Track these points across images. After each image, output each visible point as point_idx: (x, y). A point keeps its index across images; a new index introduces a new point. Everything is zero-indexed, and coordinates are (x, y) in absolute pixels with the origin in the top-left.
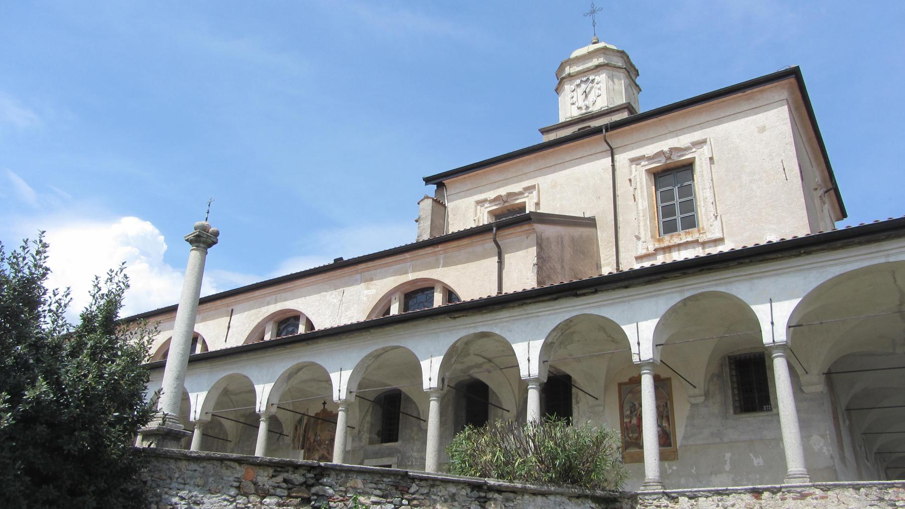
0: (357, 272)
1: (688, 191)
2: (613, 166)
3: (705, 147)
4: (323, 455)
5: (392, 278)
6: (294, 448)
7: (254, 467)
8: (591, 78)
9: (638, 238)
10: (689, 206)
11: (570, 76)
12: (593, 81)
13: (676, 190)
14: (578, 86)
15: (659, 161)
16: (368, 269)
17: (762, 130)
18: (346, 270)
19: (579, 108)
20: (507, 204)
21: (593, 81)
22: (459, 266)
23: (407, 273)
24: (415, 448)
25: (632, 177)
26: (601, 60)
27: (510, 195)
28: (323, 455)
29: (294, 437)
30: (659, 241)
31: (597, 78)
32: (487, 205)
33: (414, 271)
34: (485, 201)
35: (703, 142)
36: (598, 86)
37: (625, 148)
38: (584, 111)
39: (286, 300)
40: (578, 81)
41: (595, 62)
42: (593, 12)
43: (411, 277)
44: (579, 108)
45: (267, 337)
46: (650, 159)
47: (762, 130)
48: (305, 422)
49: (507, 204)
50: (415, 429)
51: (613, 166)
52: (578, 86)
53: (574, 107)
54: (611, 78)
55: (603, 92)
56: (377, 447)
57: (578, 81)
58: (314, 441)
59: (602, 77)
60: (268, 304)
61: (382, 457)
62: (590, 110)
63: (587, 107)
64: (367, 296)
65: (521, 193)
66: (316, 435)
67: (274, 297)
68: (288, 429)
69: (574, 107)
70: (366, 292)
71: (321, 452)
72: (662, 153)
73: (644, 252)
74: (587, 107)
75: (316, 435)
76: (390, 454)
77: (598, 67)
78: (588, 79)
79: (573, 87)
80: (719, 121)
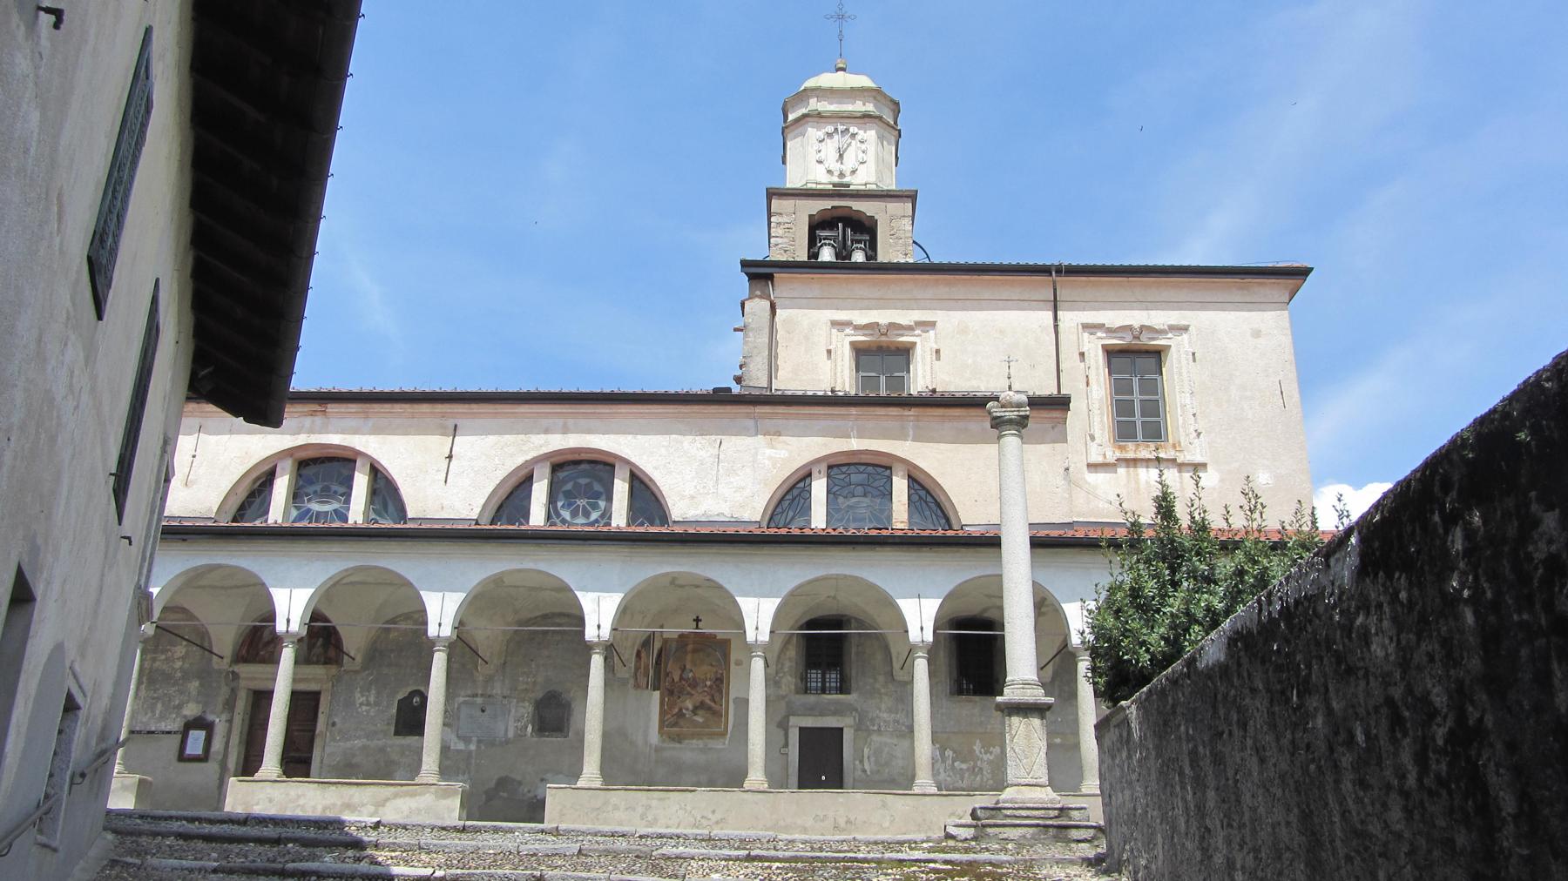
0: (748, 416)
1: (1153, 388)
2: (1056, 326)
3: (1185, 336)
4: (702, 703)
5: (820, 440)
6: (637, 686)
7: (1026, 716)
8: (853, 129)
9: (1093, 438)
10: (1154, 408)
11: (819, 116)
12: (853, 136)
13: (1136, 380)
14: (830, 135)
15: (1122, 338)
16: (771, 417)
17: (1257, 334)
18: (729, 408)
19: (829, 172)
20: (883, 338)
21: (853, 136)
22: (943, 446)
23: (849, 437)
24: (883, 706)
25: (1084, 349)
26: (870, 108)
27: (893, 326)
28: (702, 703)
29: (637, 669)
30: (1121, 448)
31: (861, 134)
32: (849, 331)
33: (860, 436)
34: (848, 324)
35: (1185, 329)
36: (863, 147)
37: (1075, 305)
38: (836, 180)
39: (589, 431)
40: (830, 129)
41: (859, 106)
42: (841, 17)
43: (855, 444)
44: (829, 172)
45: (818, 519)
46: (1110, 331)
47: (1257, 334)
48: (657, 645)
49: (883, 338)
50: (881, 678)
51: (1056, 326)
52: (830, 135)
53: (821, 169)
54: (881, 138)
55: (871, 158)
56: (811, 699)
57: (830, 129)
58: (681, 678)
59: (870, 135)
60: (547, 431)
61: (822, 715)
62: (846, 180)
63: (842, 175)
64: (770, 458)
65: (910, 328)
66: (683, 669)
67: (560, 422)
68: (629, 655)
69: (821, 169)
70: (768, 452)
71: (698, 698)
72: (1129, 328)
73: (1100, 460)
74: (842, 175)
75: (683, 669)
76: (838, 711)
77: (866, 116)
78: (847, 130)
79: (821, 134)
80: (1204, 305)
